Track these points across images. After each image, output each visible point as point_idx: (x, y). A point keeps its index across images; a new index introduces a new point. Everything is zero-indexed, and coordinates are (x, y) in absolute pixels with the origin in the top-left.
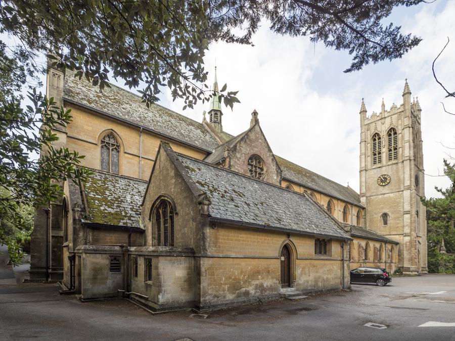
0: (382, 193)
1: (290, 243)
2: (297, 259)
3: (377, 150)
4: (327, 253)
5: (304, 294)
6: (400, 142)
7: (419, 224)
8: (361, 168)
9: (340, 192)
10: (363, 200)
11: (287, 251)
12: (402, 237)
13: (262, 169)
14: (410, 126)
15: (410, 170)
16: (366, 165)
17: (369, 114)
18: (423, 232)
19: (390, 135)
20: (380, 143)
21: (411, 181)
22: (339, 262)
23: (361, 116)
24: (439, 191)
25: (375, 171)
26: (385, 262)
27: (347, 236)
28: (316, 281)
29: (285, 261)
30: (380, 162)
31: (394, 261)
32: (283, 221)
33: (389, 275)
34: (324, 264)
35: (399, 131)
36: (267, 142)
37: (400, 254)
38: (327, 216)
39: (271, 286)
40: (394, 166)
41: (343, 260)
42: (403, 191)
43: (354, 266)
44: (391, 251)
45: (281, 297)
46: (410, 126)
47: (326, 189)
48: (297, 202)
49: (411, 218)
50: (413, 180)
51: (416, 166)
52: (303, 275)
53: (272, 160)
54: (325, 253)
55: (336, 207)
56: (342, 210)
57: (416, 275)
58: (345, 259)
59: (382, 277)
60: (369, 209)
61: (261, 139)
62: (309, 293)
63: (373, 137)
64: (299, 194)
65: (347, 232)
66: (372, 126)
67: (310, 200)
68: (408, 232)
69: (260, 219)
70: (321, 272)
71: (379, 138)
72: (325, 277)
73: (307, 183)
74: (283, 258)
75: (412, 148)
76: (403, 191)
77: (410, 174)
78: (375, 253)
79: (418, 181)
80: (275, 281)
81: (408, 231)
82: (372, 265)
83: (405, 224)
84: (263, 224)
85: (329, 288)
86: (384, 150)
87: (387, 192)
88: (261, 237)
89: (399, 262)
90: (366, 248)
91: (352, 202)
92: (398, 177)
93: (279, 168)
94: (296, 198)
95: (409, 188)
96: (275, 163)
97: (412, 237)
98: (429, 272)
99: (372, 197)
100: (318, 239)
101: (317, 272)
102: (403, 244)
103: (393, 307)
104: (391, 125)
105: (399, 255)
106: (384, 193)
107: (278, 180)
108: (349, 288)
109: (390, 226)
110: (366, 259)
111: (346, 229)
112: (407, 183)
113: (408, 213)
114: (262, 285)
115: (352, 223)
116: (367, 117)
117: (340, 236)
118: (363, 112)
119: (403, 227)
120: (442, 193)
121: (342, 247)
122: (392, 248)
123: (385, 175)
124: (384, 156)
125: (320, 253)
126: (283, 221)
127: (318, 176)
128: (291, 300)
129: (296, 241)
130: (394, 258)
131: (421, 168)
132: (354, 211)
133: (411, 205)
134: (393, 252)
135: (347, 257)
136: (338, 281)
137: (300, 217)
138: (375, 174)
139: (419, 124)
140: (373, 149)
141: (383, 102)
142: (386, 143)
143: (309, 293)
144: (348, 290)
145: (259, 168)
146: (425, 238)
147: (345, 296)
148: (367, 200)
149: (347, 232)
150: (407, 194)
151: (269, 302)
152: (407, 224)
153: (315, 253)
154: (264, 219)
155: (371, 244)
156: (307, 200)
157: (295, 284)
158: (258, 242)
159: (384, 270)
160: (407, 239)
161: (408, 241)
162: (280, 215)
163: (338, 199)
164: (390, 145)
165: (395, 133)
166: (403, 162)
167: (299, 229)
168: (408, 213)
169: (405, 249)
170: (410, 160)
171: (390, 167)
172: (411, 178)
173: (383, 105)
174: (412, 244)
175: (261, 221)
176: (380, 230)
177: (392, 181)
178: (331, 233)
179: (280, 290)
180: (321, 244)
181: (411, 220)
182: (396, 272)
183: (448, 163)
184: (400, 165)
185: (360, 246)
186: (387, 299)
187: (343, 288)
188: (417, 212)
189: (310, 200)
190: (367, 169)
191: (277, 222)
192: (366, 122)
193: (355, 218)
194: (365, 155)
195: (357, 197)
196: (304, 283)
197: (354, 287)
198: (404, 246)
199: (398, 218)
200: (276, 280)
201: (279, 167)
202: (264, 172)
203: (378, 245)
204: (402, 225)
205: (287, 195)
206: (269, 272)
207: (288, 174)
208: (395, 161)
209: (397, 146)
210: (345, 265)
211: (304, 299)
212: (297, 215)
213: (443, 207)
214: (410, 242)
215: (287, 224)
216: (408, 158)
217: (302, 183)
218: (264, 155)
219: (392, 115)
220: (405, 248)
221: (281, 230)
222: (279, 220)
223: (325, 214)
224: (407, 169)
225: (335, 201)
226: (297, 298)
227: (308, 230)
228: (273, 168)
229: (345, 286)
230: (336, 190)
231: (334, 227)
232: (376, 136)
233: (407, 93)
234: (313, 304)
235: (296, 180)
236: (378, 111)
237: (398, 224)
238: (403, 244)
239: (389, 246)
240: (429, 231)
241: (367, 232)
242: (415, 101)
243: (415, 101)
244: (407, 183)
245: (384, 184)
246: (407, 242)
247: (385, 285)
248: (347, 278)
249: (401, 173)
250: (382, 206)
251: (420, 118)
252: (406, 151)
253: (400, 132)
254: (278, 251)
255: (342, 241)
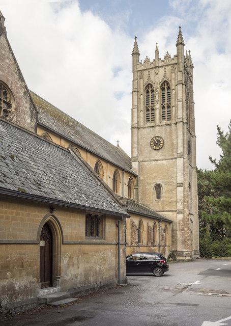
0: (155, 158)
1: (53, 220)
2: (63, 244)
3: (166, 102)
4: (100, 234)
5: (72, 296)
6: (173, 100)
7: (191, 199)
8: (133, 124)
9: (109, 152)
10: (135, 165)
11: (49, 231)
12: (175, 213)
13: (9, 105)
14: (184, 83)
15: (183, 134)
16: (138, 121)
17: (142, 58)
18: (195, 210)
19: (163, 89)
20: (153, 96)
21: (184, 147)
22: (114, 247)
23: (133, 58)
24: (212, 162)
25: (148, 130)
26: (159, 246)
27: (123, 211)
28: (87, 275)
29: (45, 247)
30: (153, 120)
31: (167, 244)
32: (44, 187)
33: (166, 262)
34: (97, 251)
35: (173, 87)
36: (18, 66)
37: (174, 235)
38: (99, 183)
39: (26, 287)
40: (168, 127)
41: (118, 244)
42: (176, 158)
43: (129, 251)
44: (165, 231)
45: (40, 304)
46: (184, 83)
47: (93, 147)
48: (60, 160)
49: (184, 192)
50: (186, 146)
51: (188, 130)
52: (71, 268)
53: (25, 93)
54: (98, 235)
55: (105, 171)
56: (112, 177)
57: (189, 261)
58: (121, 242)
59: (159, 264)
60: (141, 177)
61: (8, 58)
62: (79, 293)
63: (146, 88)
64: (63, 149)
65: (123, 206)
66: (146, 73)
67: (77, 158)
68: (182, 209)
69: (10, 181)
70: (93, 261)
71: (153, 91)
72: (98, 269)
73: (69, 135)
74: (42, 243)
75: (185, 109)
76: (176, 158)
77: (183, 139)
78: (149, 234)
79: (190, 148)
80: (31, 279)
81: (180, 206)
82: (145, 249)
83: (179, 198)
84: (16, 189)
85: (102, 284)
86: (158, 106)
87: (161, 158)
88: (11, 210)
89: (172, 244)
90: (139, 228)
91: (123, 167)
92: (171, 140)
93: (35, 108)
94: (59, 154)
95: (182, 156)
96: (28, 99)
97: (185, 214)
98: (201, 256)
99: (144, 163)
100: (90, 215)
101: (88, 262)
102: (177, 223)
103: (179, 304)
104: (164, 77)
105: (173, 236)
106: (157, 158)
107: (33, 124)
108: (125, 282)
109: (163, 201)
110: (139, 241)
111: (122, 202)
112: (180, 150)
113: (181, 185)
114: (11, 287)
115: (123, 194)
116: (140, 61)
117: (116, 211)
118: (136, 54)
119: (177, 202)
120: (216, 165)
121: (118, 226)
122: (166, 227)
123: (158, 137)
124: (158, 113)
125: (92, 234)
126: (44, 187)
127: (83, 128)
128: (54, 306)
129: (61, 217)
130: (167, 240)
131: (193, 134)
132: (125, 179)
133: (184, 176)
134: (166, 233)
135: (123, 239)
136: (112, 273)
137: (66, 182)
138: (148, 134)
139: (192, 83)
140: (146, 103)
141: (157, 47)
142: (159, 99)
143: (79, 293)
144: (124, 285)
145: (4, 102)
146: (196, 216)
147: (122, 293)
148: (139, 166)
149: (123, 206)
150: (180, 162)
151: (23, 313)
152: (181, 198)
153: (86, 235)
154: (16, 182)
155: (145, 222)
156: (73, 158)
157: (60, 281)
158: (7, 218)
159: (161, 256)
160: (180, 216)
161: (181, 219)
162: (39, 177)
163: (107, 162)
164: (163, 101)
165: (169, 88)
166: (176, 124)
167: (66, 200)
168: (181, 185)
169: (178, 229)
170: (183, 123)
171: (164, 127)
172: (184, 144)
173: (157, 52)
174: (186, 223)
175: (13, 184)
176: (153, 204)
177: (166, 146)
178: (105, 207)
179: (39, 292)
180: (92, 222)
181: (184, 195)
182: (170, 257)
183: (221, 131)
184: (173, 126)
185: (133, 225)
186: (169, 294)
187: (119, 282)
188: (190, 184)
189: (77, 158)
190: (139, 127)
191: (36, 188)
192: (139, 68)
193: (126, 188)
194: (138, 108)
195: (129, 161)
196: (71, 279)
197: (132, 280)
198: (178, 224)
199: (171, 190)
200: (34, 277)
201: (34, 106)
202: (12, 109)
203: (151, 224)
204: (175, 200)
205: (45, 148)
206: (22, 266)
207: (44, 119)
208: (168, 122)
209: (170, 104)
210: (121, 251)
211: (73, 302)
212: (62, 179)
213: (216, 181)
214: (184, 220)
215: (49, 191)
216: (181, 120)
217: (58, 131)
218: (13, 84)
219: (166, 66)
220: (178, 227)
221: (41, 200)
222: (39, 185)
223: (97, 180)
224: (180, 133)
225: (104, 164)
226: (63, 302)
227: (77, 202)
228: (26, 106)
229: (121, 279)
230: (105, 150)
231: (108, 199)
232: (149, 87)
233: (180, 44)
234: (86, 309)
235: (55, 128)
236: (152, 58)
237: (171, 198)
238: (177, 223)
239: (163, 225)
240: (200, 208)
241: (139, 206)
242: (188, 55)
243: (188, 55)
244: (180, 150)
245: (157, 148)
246: (180, 221)
247: (162, 276)
248: (123, 270)
249: (174, 137)
250: (154, 175)
251: (192, 76)
252: (179, 112)
253: (173, 87)
254: (36, 233)
255: (118, 219)
